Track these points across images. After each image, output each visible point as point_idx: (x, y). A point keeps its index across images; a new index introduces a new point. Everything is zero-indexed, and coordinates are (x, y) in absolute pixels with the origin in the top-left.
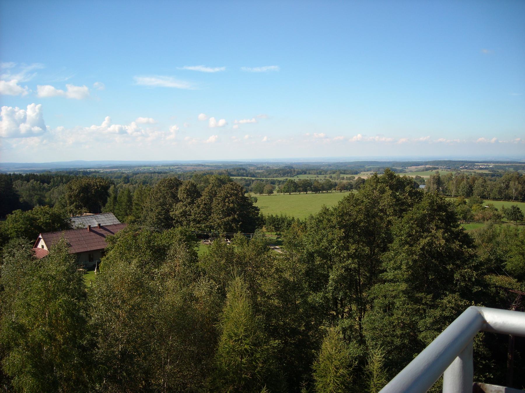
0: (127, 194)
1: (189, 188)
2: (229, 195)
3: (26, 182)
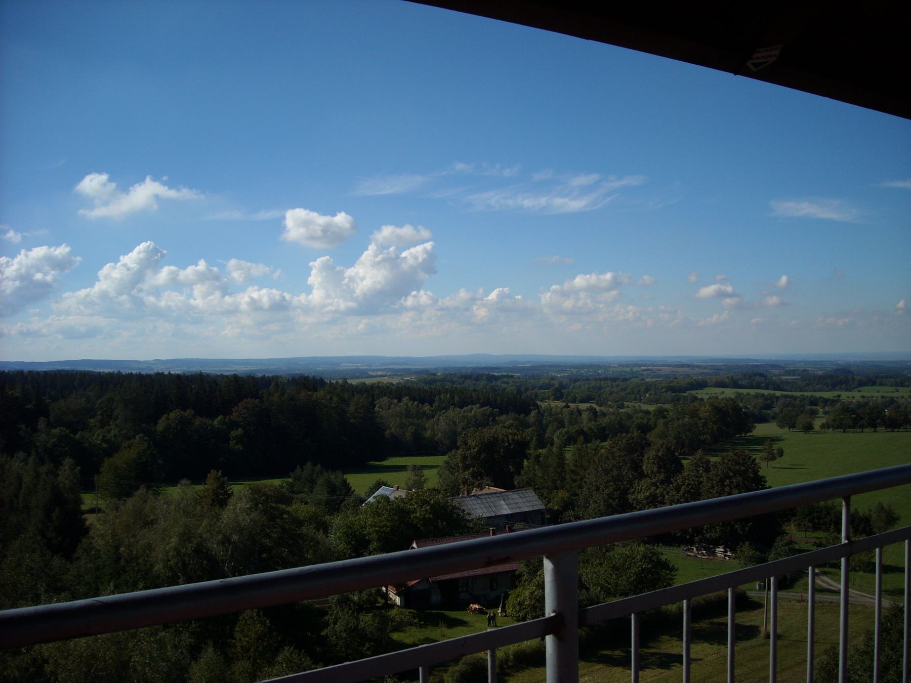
0: (557, 453)
1: (663, 455)
2: (731, 474)
3: (396, 400)
